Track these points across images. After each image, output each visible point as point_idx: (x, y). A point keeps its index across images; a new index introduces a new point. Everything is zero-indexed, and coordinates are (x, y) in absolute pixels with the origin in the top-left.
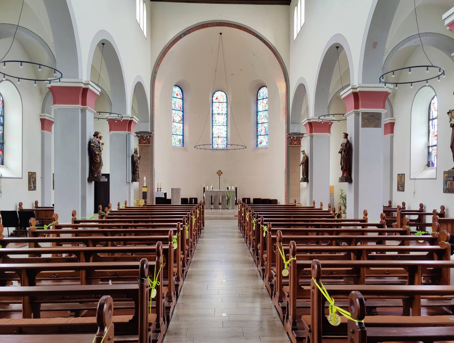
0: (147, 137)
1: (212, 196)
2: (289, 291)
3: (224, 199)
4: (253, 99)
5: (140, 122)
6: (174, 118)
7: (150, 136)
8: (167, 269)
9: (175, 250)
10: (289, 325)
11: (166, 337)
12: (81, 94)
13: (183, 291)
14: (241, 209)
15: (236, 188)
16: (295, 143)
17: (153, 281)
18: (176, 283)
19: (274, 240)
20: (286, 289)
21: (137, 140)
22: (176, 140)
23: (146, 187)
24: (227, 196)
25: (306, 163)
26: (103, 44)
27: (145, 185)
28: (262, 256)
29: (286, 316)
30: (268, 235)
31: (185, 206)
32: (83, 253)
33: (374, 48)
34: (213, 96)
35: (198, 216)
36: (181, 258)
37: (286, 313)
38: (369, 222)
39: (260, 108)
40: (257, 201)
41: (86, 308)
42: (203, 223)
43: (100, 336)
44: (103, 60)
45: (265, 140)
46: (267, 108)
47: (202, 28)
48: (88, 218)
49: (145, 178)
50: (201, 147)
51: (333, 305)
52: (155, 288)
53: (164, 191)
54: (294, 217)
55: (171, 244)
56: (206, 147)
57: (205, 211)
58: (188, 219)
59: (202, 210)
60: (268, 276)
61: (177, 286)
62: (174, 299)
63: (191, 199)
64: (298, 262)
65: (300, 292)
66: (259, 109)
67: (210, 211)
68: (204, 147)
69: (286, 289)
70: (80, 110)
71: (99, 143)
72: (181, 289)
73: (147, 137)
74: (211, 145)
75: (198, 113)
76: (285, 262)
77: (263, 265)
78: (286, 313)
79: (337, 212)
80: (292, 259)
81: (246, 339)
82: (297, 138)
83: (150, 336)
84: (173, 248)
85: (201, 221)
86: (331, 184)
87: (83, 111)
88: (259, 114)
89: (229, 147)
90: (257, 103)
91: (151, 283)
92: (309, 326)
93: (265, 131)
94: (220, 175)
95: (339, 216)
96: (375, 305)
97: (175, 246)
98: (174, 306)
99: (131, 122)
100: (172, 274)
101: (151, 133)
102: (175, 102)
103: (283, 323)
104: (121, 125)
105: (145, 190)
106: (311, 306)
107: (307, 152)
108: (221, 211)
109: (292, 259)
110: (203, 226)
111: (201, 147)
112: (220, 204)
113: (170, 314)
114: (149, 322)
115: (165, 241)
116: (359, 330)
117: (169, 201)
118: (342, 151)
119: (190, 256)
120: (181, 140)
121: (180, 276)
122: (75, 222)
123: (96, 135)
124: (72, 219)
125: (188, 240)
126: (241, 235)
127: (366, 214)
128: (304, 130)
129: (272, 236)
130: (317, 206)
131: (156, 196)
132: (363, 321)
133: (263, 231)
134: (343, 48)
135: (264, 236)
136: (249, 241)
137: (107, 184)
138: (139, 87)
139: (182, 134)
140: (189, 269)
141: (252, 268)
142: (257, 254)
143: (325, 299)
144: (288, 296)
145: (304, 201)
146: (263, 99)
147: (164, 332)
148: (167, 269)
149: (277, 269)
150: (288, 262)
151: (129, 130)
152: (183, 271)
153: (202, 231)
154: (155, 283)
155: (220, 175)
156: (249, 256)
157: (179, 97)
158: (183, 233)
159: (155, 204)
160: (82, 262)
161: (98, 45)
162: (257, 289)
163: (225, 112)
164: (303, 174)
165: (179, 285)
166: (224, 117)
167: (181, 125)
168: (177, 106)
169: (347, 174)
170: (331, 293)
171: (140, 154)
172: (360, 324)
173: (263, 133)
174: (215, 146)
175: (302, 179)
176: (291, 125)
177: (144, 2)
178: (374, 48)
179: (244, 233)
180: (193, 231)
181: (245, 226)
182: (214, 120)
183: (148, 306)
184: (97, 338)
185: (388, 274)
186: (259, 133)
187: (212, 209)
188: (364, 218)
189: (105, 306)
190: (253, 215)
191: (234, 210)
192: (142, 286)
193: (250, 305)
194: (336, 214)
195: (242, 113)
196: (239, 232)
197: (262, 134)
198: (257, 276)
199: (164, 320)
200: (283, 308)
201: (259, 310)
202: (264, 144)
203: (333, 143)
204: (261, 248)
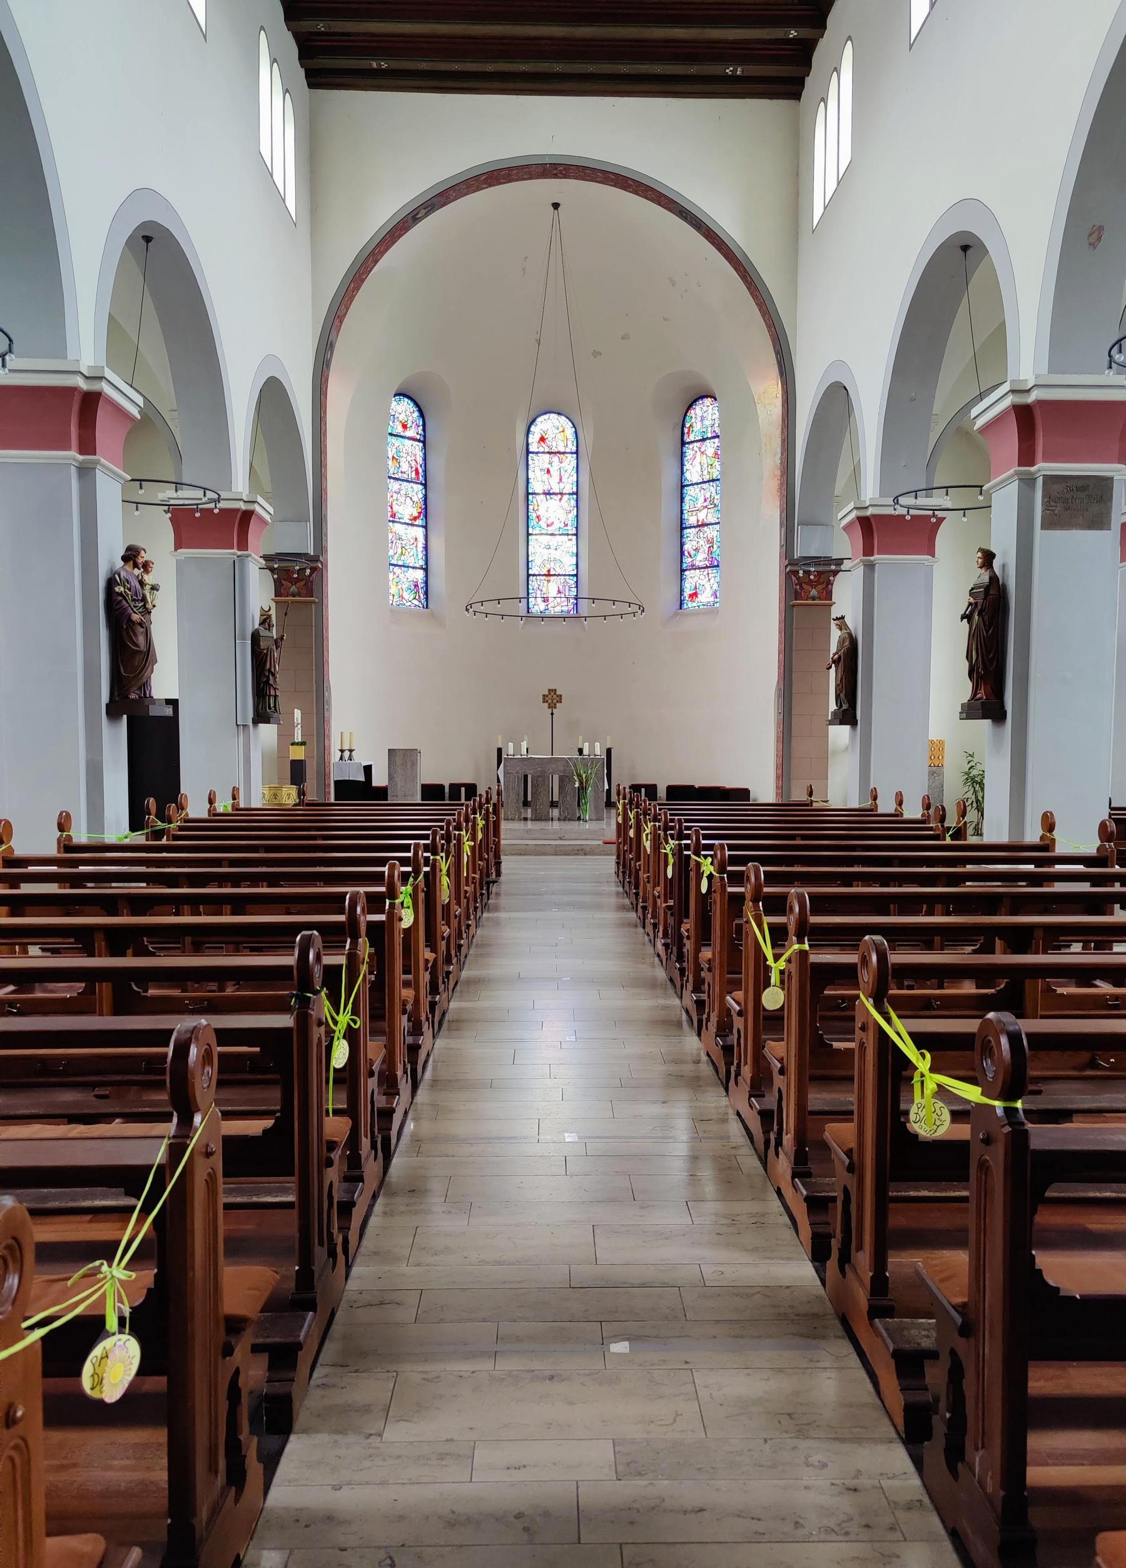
0: (303, 570)
1: (526, 777)
2: (784, 1054)
3: (568, 787)
4: (667, 442)
5: (279, 519)
6: (395, 508)
7: (313, 570)
8: (380, 990)
9: (407, 931)
10: (783, 1165)
11: (380, 1201)
12: (75, 414)
13: (435, 1069)
14: (626, 818)
15: (609, 751)
16: (814, 592)
17: (338, 1013)
18: (410, 1040)
19: (739, 899)
20: (777, 1050)
21: (268, 579)
22: (402, 585)
23: (303, 744)
24: (579, 776)
25: (849, 660)
26: (148, 239)
27: (298, 738)
28: (696, 958)
29: (772, 1136)
30: (717, 885)
31: (433, 807)
32: (102, 936)
33: (1093, 245)
34: (528, 431)
35: (480, 836)
36: (427, 961)
37: (775, 1128)
38: (1060, 849)
39: (693, 473)
40: (677, 793)
41: (117, 1110)
42: (498, 864)
43: (180, 1140)
44: (147, 294)
45: (707, 586)
46: (715, 474)
47: (490, 185)
48: (110, 838)
49: (298, 714)
50: (487, 607)
51: (926, 1072)
52: (344, 1037)
53: (362, 758)
54: (804, 837)
55: (392, 906)
56: (505, 607)
57: (504, 825)
58: (449, 841)
59: (492, 818)
60: (714, 1018)
61: (414, 1049)
62: (404, 1086)
63: (455, 788)
64: (814, 958)
65: (821, 1064)
66: (687, 475)
67: (518, 826)
68: (498, 608)
69: (777, 1050)
70: (73, 470)
71: (142, 583)
72: (426, 1062)
73: (303, 570)
74: (524, 601)
75: (476, 496)
76: (770, 961)
77: (697, 989)
78: (775, 1128)
79: (951, 821)
80: (796, 947)
81: (642, 1208)
82: (820, 573)
83: (331, 1183)
84: (401, 919)
85: (490, 854)
86: (934, 735)
87: (86, 473)
88: (690, 492)
89: (585, 607)
90: (682, 455)
91: (333, 1018)
92: (849, 1153)
93: (710, 552)
94: (552, 706)
95: (959, 833)
96: (1070, 1106)
97: (407, 919)
98: (406, 1113)
99: (247, 515)
100: (398, 1008)
101: (315, 559)
102: (398, 451)
103: (764, 1162)
104: (213, 526)
105: (298, 753)
106: (855, 1108)
107: (854, 622)
108: (556, 825)
109: (796, 947)
110: (498, 874)
111: (487, 607)
112: (553, 804)
113: (394, 1133)
114: (326, 1137)
115: (375, 903)
116: (1008, 1129)
117: (381, 793)
118: (972, 613)
119: (454, 961)
120: (421, 585)
121: (423, 1018)
122: (67, 846)
123: (131, 555)
124: (59, 841)
125: (447, 908)
126: (627, 901)
127: (1049, 823)
128: (843, 545)
129: (730, 889)
130: (886, 806)
131: (335, 776)
132: (1019, 1104)
133: (699, 876)
134: (984, 251)
135: (704, 889)
136: (653, 917)
137: (172, 724)
138: (272, 396)
139: (422, 563)
140: (452, 1005)
141: (661, 1002)
142: (680, 957)
143: (906, 1064)
144: (782, 1072)
145: (841, 790)
146: (703, 440)
147: (375, 1186)
148: (380, 990)
149: (746, 992)
150: (782, 964)
151: (243, 545)
152: (433, 1005)
153: (494, 889)
154: (344, 1019)
155: (552, 706)
156: (653, 966)
157: (410, 433)
158: (431, 880)
159: (332, 800)
160: (100, 956)
161: (130, 242)
162: (676, 1062)
163: (569, 486)
164: (837, 697)
165: (419, 1047)
166: (569, 503)
167: (419, 532)
168: (405, 467)
169: (991, 686)
170: (921, 1040)
171: (281, 626)
172: (1010, 1112)
173: (700, 559)
174: (538, 607)
175: (835, 713)
176: (799, 530)
177: (286, 91)
178: (1093, 245)
179: (637, 894)
180: (463, 881)
181: (637, 871)
182: (533, 515)
183: (325, 1107)
184: (170, 1146)
185: (1116, 1007)
186: (687, 560)
187: (526, 819)
188: (1042, 838)
189: (193, 1051)
190: (665, 831)
191: (603, 824)
192: (303, 1020)
193: (656, 1110)
194: (949, 829)
195: (629, 489)
196: (618, 893)
197: (698, 564)
198: (679, 1024)
199: (374, 1146)
200: (766, 1116)
201: (682, 1129)
202: (705, 597)
203: (946, 585)
204: (692, 933)
